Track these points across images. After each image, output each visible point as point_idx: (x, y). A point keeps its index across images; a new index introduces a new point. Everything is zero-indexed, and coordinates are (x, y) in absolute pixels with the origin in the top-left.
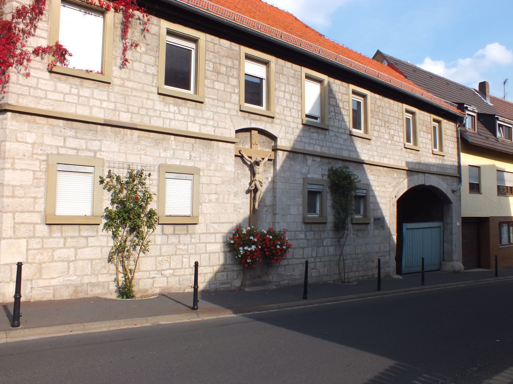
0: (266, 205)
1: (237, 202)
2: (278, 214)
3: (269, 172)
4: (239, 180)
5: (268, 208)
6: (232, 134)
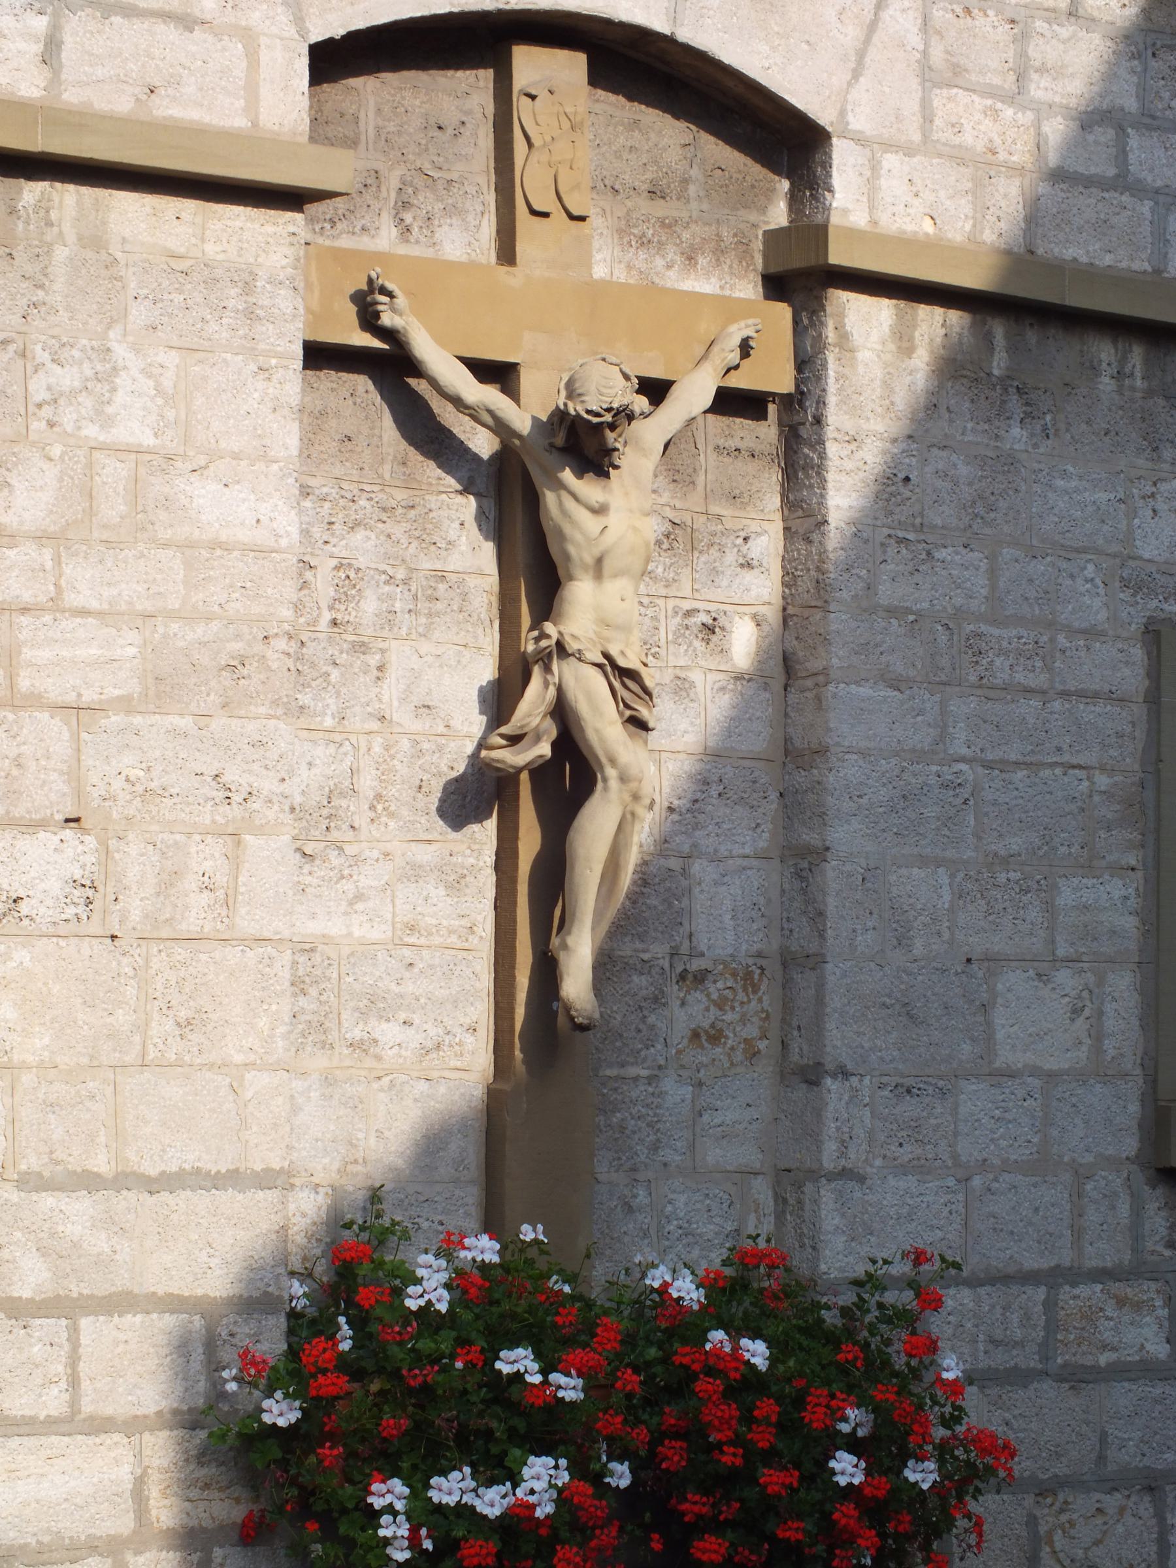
0: (696, 965)
1: (335, 928)
3: (731, 557)
4: (361, 648)
6: (265, 91)
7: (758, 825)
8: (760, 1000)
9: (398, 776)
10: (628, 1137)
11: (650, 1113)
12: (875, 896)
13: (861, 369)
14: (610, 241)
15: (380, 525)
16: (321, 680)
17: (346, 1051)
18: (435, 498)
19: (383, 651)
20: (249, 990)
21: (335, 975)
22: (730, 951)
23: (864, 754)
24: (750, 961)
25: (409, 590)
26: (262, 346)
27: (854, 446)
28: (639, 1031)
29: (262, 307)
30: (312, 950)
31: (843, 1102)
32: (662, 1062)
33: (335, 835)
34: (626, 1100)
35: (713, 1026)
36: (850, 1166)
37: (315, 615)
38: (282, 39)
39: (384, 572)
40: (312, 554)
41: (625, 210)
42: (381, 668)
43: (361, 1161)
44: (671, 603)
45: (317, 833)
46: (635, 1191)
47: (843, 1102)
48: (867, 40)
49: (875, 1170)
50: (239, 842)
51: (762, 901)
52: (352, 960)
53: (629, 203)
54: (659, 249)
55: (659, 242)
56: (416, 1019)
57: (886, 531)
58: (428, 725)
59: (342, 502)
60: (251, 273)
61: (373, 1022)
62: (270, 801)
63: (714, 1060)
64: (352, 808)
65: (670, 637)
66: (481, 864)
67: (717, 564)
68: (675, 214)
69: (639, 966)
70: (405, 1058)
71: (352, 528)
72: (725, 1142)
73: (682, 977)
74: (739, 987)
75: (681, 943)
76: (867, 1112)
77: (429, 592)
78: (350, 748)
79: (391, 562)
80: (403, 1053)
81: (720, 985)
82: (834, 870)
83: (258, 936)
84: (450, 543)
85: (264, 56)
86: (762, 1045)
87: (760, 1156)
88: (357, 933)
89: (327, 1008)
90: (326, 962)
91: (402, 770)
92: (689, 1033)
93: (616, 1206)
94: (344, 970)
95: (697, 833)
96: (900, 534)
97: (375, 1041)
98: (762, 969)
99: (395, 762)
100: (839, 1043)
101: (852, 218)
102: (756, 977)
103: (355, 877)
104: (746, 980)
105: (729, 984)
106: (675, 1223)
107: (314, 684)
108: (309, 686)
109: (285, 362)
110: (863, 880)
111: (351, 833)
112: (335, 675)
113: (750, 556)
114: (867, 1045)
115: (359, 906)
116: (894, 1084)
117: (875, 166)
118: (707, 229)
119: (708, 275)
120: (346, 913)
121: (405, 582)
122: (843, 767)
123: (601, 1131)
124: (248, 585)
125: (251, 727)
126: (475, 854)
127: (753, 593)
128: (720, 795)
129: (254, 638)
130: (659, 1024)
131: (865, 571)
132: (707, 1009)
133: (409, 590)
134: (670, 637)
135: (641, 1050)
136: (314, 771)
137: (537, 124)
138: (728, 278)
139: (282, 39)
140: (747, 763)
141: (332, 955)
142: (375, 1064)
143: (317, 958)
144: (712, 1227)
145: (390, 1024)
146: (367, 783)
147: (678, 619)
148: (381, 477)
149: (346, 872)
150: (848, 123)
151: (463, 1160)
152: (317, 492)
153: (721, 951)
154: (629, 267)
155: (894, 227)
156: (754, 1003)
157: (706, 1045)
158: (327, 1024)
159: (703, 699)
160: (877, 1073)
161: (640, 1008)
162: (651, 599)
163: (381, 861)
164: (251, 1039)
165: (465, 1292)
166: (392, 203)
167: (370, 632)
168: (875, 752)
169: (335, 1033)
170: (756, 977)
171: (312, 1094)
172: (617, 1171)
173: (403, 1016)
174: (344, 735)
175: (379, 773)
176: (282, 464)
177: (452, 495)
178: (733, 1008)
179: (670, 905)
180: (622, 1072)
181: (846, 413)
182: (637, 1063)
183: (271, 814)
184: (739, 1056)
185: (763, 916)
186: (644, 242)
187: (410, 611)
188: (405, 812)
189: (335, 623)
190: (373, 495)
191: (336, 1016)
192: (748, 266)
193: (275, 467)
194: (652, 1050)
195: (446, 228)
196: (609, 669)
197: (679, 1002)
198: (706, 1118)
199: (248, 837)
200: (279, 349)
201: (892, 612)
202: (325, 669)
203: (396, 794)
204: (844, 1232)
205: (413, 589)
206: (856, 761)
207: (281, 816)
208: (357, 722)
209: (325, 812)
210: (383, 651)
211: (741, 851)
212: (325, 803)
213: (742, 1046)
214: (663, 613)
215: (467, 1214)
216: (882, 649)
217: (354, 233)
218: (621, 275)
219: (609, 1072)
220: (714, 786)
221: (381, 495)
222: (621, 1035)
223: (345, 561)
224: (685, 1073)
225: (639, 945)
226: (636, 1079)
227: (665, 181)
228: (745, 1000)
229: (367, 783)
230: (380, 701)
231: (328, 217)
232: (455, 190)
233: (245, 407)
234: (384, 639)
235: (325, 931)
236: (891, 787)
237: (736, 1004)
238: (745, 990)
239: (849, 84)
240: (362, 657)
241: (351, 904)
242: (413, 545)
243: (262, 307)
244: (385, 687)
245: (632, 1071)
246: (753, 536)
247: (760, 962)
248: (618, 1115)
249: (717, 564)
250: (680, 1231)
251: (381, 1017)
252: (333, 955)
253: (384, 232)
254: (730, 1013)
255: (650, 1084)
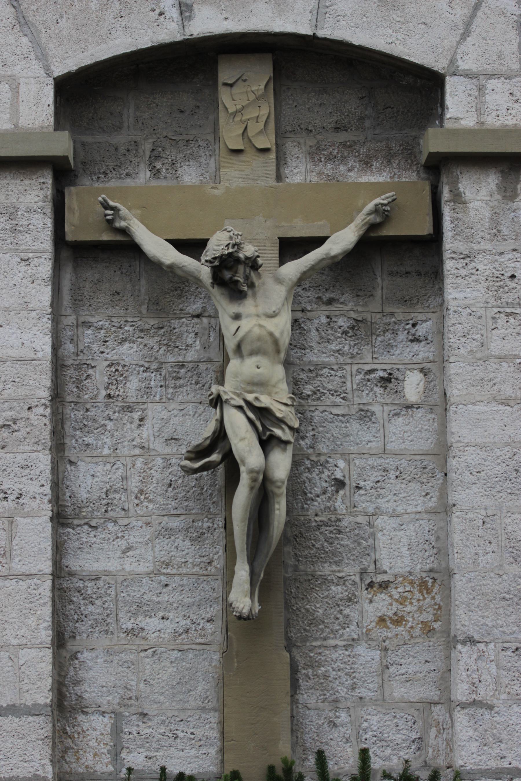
0: (380, 578)
1: (113, 565)
2: (471, 641)
3: (402, 336)
4: (129, 409)
5: (402, 601)
6: (22, 108)
7: (427, 494)
8: (433, 598)
9: (154, 479)
10: (330, 682)
11: (347, 667)
12: (493, 532)
13: (472, 213)
14: (304, 160)
15: (140, 340)
16: (100, 429)
17: (122, 635)
18: (177, 321)
19: (143, 410)
20: (22, 603)
21: (113, 593)
22: (408, 569)
23: (481, 447)
24: (424, 575)
25: (160, 374)
26: (22, 247)
27: (467, 260)
28: (338, 619)
29: (22, 226)
30: (97, 579)
31: (472, 659)
32: (356, 637)
33: (111, 514)
34: (328, 660)
35: (395, 614)
36: (480, 699)
37: (95, 393)
38: (35, 78)
39: (142, 366)
40: (92, 359)
41: (316, 141)
42: (141, 420)
43: (134, 698)
44: (355, 368)
45: (99, 514)
46: (337, 714)
47: (472, 659)
48: (473, 15)
49: (501, 702)
50: (12, 522)
51: (433, 538)
52: (125, 584)
53: (319, 137)
54: (342, 161)
55: (341, 156)
56: (171, 615)
57: (496, 310)
58: (175, 449)
59: (113, 329)
60: (14, 208)
61: (140, 618)
62: (35, 498)
63: (397, 635)
64: (123, 499)
65: (355, 387)
66: (216, 526)
67: (391, 341)
68: (355, 138)
69: (335, 581)
70: (164, 639)
71: (121, 343)
72: (408, 684)
73: (371, 585)
74: (416, 591)
75: (369, 566)
76: (493, 665)
77: (174, 375)
78: (121, 465)
79: (147, 359)
80: (162, 635)
81: (400, 590)
82: (458, 517)
83: (27, 573)
84: (187, 346)
85: (22, 89)
86: (436, 625)
87: (438, 693)
88: (128, 568)
89: (109, 612)
90: (107, 586)
91: (157, 476)
92: (377, 619)
93: (323, 723)
94: (119, 589)
95: (379, 501)
96: (508, 310)
97: (143, 629)
98: (435, 580)
99: (152, 471)
100: (467, 623)
101: (463, 122)
102: (430, 584)
103: (126, 537)
104: (421, 586)
105: (407, 589)
106: (371, 733)
107: (95, 431)
108: (93, 433)
109: (38, 255)
110: (484, 523)
111: (123, 512)
112: (110, 425)
113: (417, 335)
114: (490, 624)
115: (130, 553)
116: (514, 648)
117: (481, 89)
118: (379, 144)
119: (380, 171)
120: (120, 558)
121: (158, 370)
122: (464, 456)
123: (309, 678)
124: (17, 380)
125: (19, 458)
126: (211, 521)
127: (420, 356)
128: (397, 477)
129: (22, 408)
130: (352, 614)
131: (479, 336)
132: (391, 604)
133: (160, 374)
134: (355, 387)
135: (339, 629)
136: (96, 479)
137: (233, 100)
138: (396, 171)
139: (35, 78)
140: (418, 457)
141: (111, 582)
142: (143, 642)
143: (101, 583)
144: (400, 736)
145: (153, 619)
146: (134, 484)
147: (361, 376)
148: (140, 312)
149: (120, 535)
150: (458, 67)
151: (207, 697)
152: (95, 325)
153: (400, 570)
154: (319, 174)
155: (498, 124)
156: (428, 600)
157: (391, 626)
158: (109, 620)
159: (382, 422)
160: (500, 641)
161: (338, 605)
162: (339, 366)
163: (144, 527)
164: (23, 631)
165: (68, 773)
166: (147, 158)
167: (134, 399)
168: (490, 445)
169: (114, 625)
170: (430, 584)
171: (98, 661)
172: (323, 702)
173: (161, 614)
174: (117, 459)
175: (141, 478)
176: (38, 311)
177: (190, 319)
178: (411, 603)
179: (359, 544)
180: (325, 643)
181: (460, 241)
182: (336, 638)
183: (34, 504)
184: (417, 631)
185: (433, 547)
186: (331, 158)
187: (161, 386)
188: (160, 500)
189: (109, 396)
190: (134, 324)
191: (115, 616)
192: (412, 162)
193: (34, 314)
194: (348, 629)
195: (186, 167)
196: (245, 408)
197: (368, 601)
198: (392, 669)
199: (18, 519)
200: (34, 247)
201: (501, 358)
202: (102, 423)
203: (153, 490)
204: (477, 740)
205: (163, 374)
206: (474, 451)
207: (42, 506)
208: (125, 450)
209: (104, 502)
210: (143, 410)
211: (414, 510)
212: (104, 497)
213: (420, 626)
214: (349, 373)
215: (211, 728)
216: (494, 382)
217: (120, 178)
218: (314, 178)
219: (314, 644)
220: (392, 472)
221: (140, 323)
222: (323, 622)
223: (114, 362)
224: (373, 644)
225: (334, 568)
226: (335, 647)
227: (346, 120)
228: (421, 598)
229: (134, 484)
230: (141, 438)
231: (102, 171)
232: (192, 145)
233: (13, 282)
234: (144, 403)
235: (106, 569)
236: (504, 465)
237: (414, 601)
238: (420, 592)
239: (459, 43)
240: (129, 414)
241: (124, 553)
242: (162, 349)
243: (22, 226)
244: (145, 429)
245: (332, 642)
246: (420, 322)
247: (432, 575)
248: (322, 669)
249: (391, 341)
250: (375, 739)
251: (147, 616)
252: (112, 582)
253: (142, 175)
254: (409, 606)
255: (346, 650)
